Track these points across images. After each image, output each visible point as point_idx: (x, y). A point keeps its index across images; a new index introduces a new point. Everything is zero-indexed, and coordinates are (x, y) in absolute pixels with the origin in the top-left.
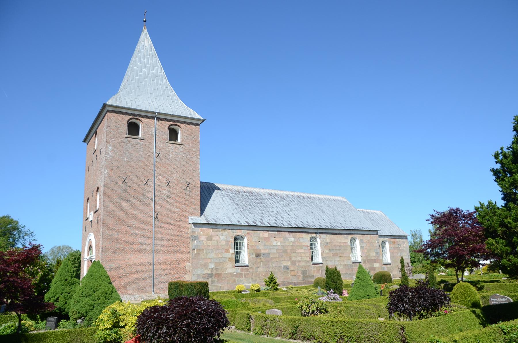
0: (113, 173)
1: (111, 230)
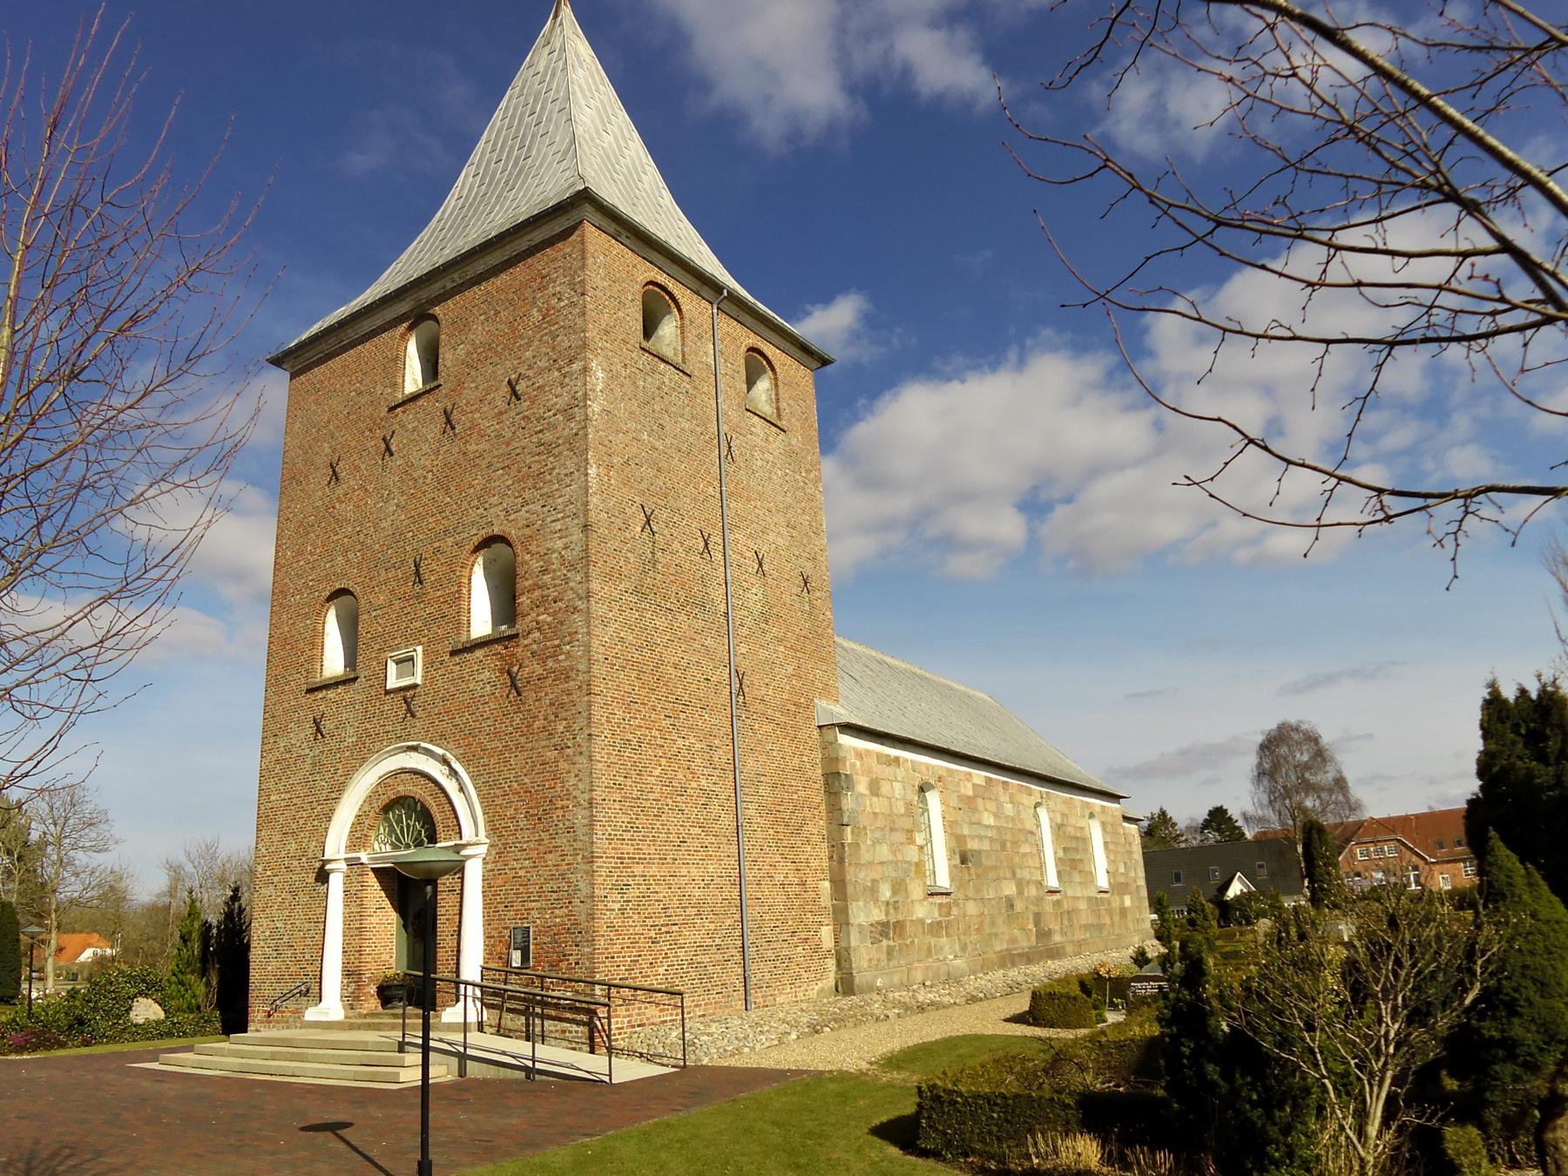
0: (613, 482)
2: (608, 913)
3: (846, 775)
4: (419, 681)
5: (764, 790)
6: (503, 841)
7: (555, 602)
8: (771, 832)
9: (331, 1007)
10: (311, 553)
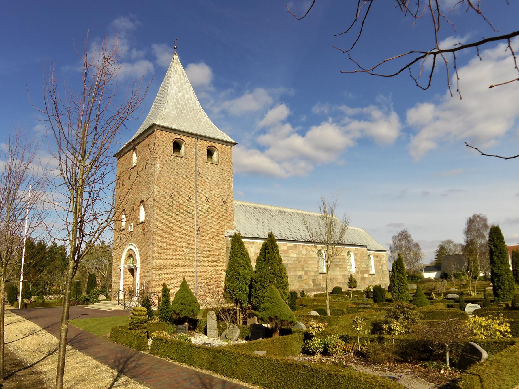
8: (207, 261)
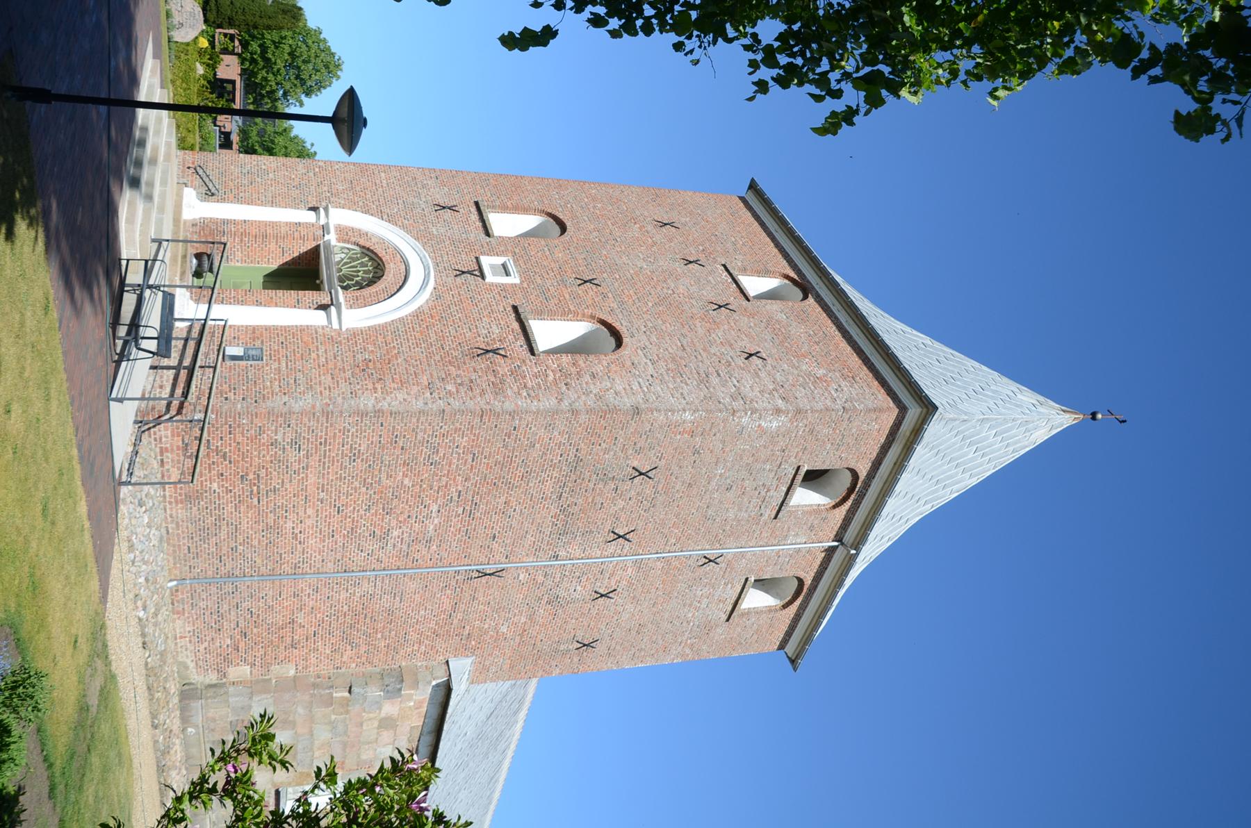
0: (679, 437)
1: (453, 441)
2: (273, 428)
3: (400, 690)
4: (487, 280)
5: (386, 602)
6: (344, 341)
7: (566, 384)
8: (346, 608)
9: (196, 208)
10: (594, 207)
